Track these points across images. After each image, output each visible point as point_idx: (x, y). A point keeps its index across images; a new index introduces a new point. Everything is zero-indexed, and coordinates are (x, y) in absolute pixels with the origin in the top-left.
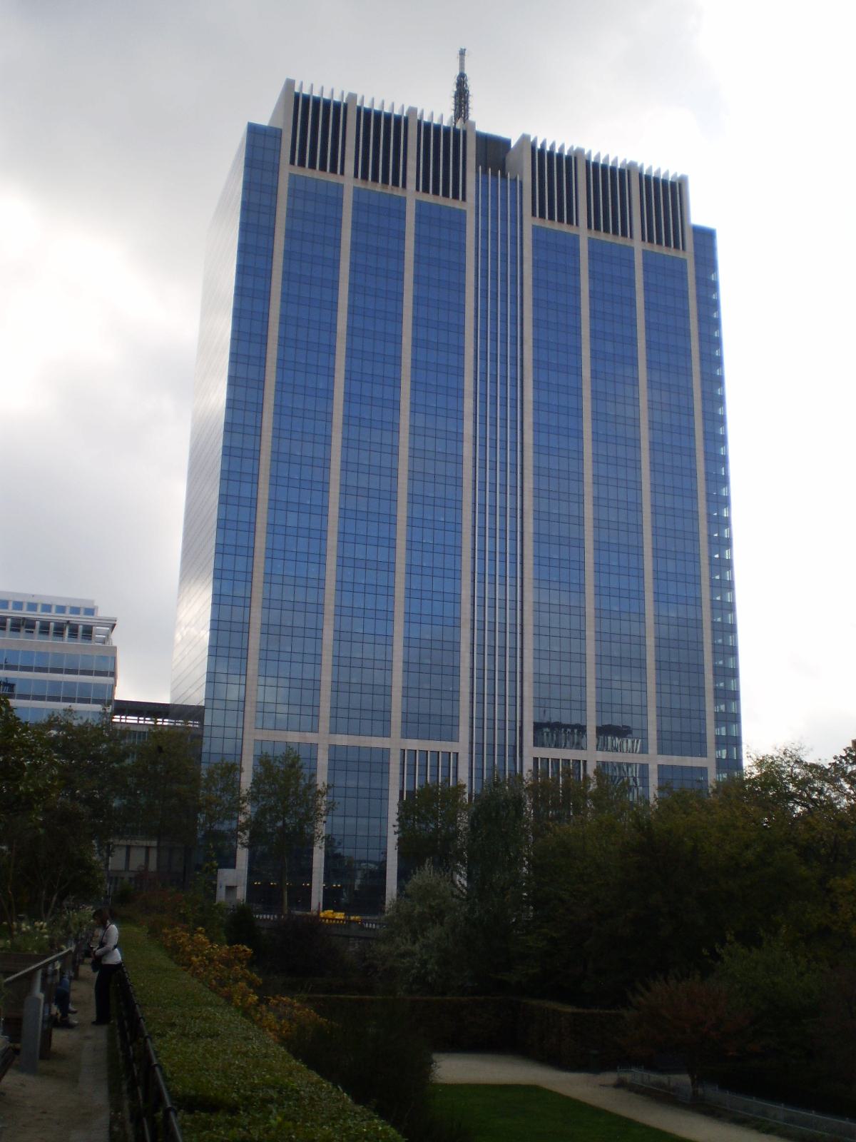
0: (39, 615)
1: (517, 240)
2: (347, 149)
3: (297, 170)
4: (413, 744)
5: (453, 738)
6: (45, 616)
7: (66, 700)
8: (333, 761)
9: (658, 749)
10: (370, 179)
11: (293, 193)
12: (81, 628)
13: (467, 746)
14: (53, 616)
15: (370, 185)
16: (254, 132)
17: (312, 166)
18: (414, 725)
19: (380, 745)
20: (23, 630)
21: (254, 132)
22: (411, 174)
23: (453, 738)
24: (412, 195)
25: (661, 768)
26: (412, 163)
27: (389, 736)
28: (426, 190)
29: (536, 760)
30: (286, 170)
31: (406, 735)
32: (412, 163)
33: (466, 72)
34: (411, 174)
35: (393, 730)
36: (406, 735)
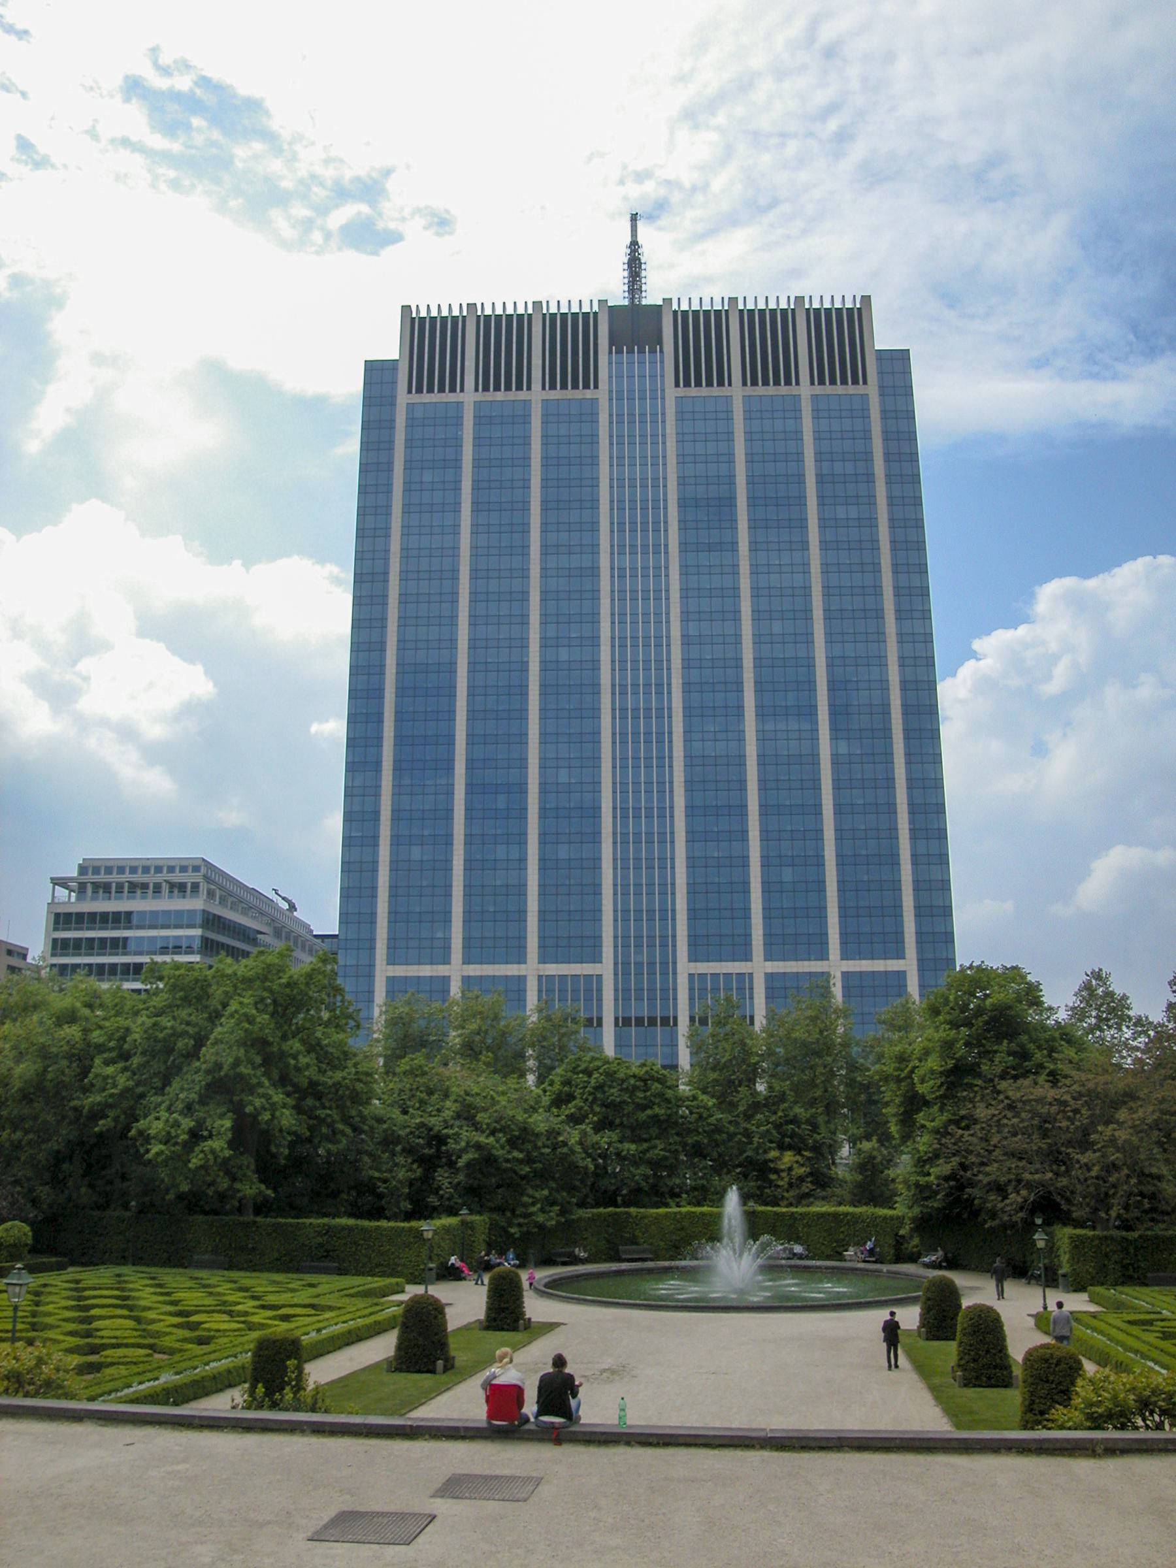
0: (115, 878)
1: (657, 418)
2: (467, 364)
3: (682, 391)
4: (552, 969)
5: (596, 958)
6: (159, 878)
7: (149, 953)
8: (846, 988)
9: (842, 953)
10: (492, 388)
11: (681, 416)
12: (189, 885)
13: (612, 966)
14: (127, 877)
15: (828, 389)
16: (372, 368)
17: (844, 382)
18: (775, 947)
19: (516, 973)
20: (139, 891)
21: (372, 368)
22: (537, 374)
23: (596, 958)
24: (469, 397)
25: (846, 975)
26: (537, 361)
27: (601, 962)
28: (822, 382)
29: (691, 976)
30: (403, 399)
31: (543, 960)
32: (537, 361)
33: (640, 240)
34: (537, 374)
35: (453, 956)
36: (543, 960)
